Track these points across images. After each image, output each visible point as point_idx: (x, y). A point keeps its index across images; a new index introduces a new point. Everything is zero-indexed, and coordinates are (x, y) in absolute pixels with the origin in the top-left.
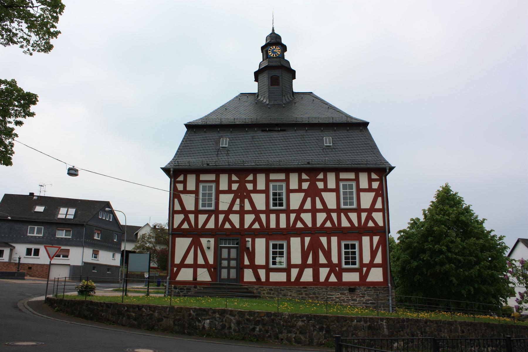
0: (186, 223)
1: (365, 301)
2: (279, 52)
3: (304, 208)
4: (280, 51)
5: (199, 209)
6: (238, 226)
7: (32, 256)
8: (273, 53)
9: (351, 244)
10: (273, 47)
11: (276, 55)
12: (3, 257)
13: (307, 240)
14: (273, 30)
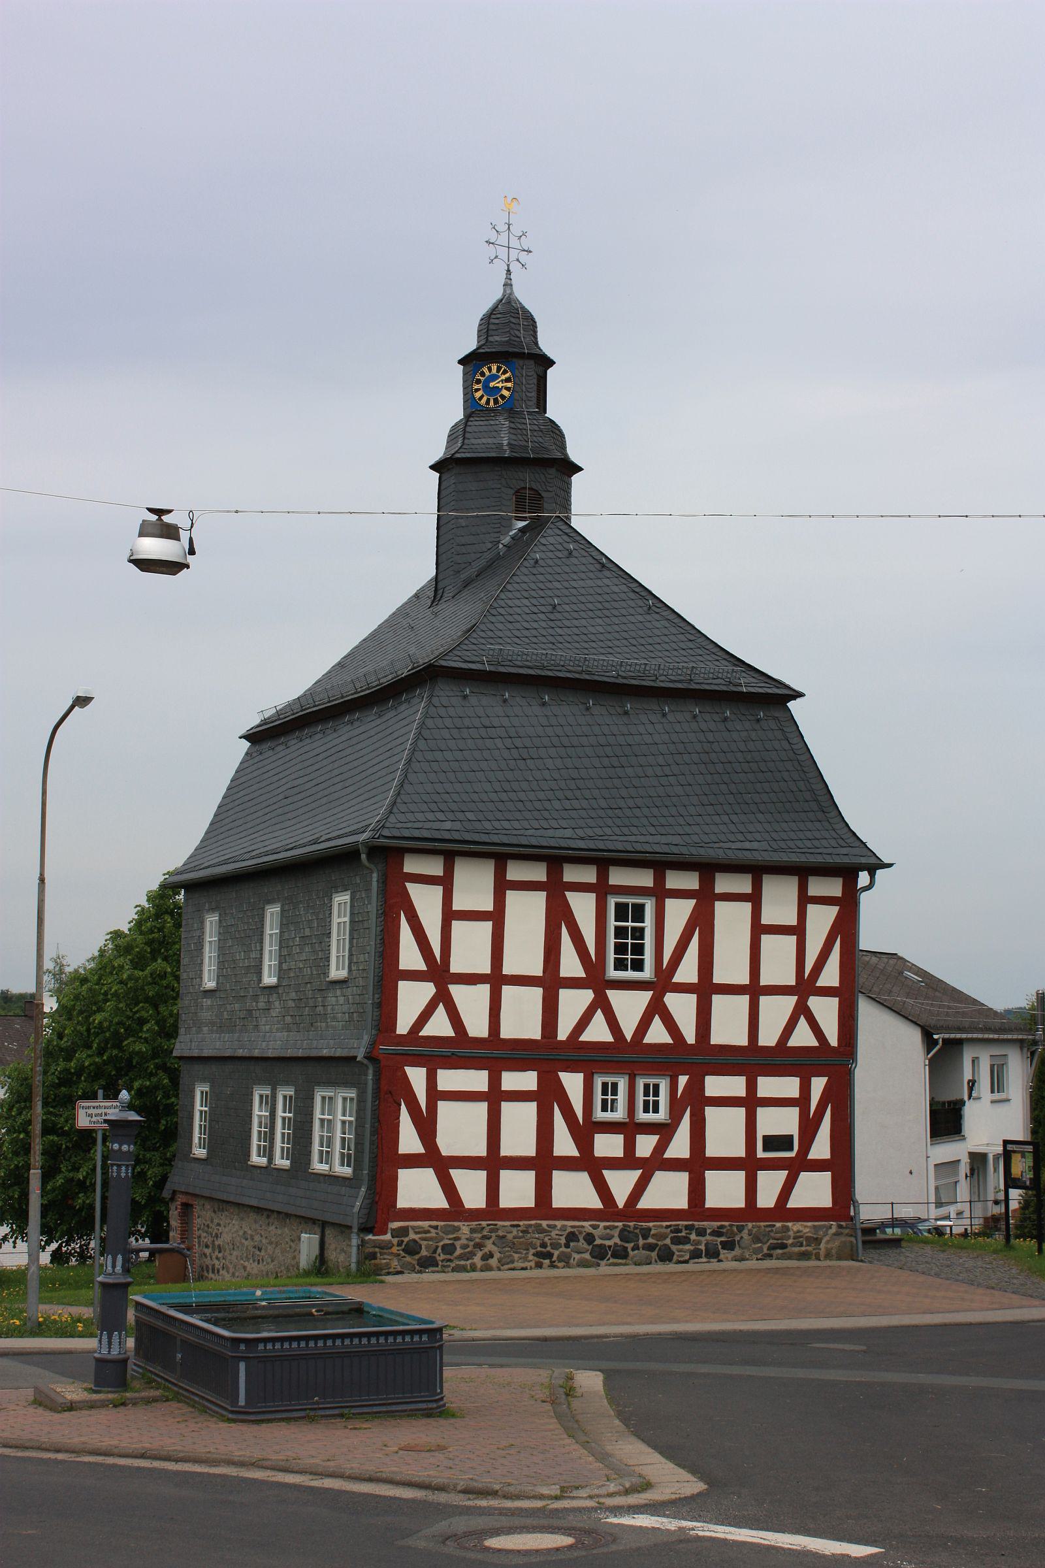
0: (657, 1022)
1: (768, 1250)
2: (508, 389)
3: (675, 979)
4: (509, 385)
5: (607, 975)
6: (690, 1037)
7: (609, 1112)
8: (487, 395)
9: (612, 1083)
10: (490, 369)
11: (496, 401)
12: (792, 1136)
13: (683, 1080)
14: (508, 285)
